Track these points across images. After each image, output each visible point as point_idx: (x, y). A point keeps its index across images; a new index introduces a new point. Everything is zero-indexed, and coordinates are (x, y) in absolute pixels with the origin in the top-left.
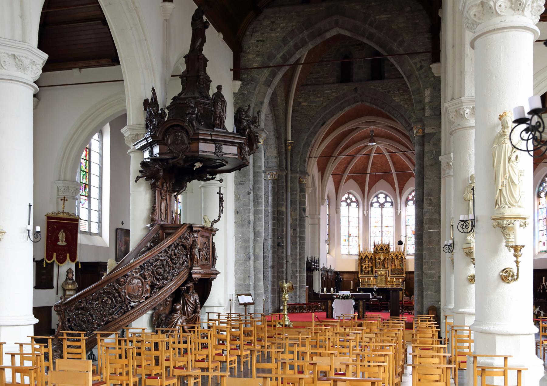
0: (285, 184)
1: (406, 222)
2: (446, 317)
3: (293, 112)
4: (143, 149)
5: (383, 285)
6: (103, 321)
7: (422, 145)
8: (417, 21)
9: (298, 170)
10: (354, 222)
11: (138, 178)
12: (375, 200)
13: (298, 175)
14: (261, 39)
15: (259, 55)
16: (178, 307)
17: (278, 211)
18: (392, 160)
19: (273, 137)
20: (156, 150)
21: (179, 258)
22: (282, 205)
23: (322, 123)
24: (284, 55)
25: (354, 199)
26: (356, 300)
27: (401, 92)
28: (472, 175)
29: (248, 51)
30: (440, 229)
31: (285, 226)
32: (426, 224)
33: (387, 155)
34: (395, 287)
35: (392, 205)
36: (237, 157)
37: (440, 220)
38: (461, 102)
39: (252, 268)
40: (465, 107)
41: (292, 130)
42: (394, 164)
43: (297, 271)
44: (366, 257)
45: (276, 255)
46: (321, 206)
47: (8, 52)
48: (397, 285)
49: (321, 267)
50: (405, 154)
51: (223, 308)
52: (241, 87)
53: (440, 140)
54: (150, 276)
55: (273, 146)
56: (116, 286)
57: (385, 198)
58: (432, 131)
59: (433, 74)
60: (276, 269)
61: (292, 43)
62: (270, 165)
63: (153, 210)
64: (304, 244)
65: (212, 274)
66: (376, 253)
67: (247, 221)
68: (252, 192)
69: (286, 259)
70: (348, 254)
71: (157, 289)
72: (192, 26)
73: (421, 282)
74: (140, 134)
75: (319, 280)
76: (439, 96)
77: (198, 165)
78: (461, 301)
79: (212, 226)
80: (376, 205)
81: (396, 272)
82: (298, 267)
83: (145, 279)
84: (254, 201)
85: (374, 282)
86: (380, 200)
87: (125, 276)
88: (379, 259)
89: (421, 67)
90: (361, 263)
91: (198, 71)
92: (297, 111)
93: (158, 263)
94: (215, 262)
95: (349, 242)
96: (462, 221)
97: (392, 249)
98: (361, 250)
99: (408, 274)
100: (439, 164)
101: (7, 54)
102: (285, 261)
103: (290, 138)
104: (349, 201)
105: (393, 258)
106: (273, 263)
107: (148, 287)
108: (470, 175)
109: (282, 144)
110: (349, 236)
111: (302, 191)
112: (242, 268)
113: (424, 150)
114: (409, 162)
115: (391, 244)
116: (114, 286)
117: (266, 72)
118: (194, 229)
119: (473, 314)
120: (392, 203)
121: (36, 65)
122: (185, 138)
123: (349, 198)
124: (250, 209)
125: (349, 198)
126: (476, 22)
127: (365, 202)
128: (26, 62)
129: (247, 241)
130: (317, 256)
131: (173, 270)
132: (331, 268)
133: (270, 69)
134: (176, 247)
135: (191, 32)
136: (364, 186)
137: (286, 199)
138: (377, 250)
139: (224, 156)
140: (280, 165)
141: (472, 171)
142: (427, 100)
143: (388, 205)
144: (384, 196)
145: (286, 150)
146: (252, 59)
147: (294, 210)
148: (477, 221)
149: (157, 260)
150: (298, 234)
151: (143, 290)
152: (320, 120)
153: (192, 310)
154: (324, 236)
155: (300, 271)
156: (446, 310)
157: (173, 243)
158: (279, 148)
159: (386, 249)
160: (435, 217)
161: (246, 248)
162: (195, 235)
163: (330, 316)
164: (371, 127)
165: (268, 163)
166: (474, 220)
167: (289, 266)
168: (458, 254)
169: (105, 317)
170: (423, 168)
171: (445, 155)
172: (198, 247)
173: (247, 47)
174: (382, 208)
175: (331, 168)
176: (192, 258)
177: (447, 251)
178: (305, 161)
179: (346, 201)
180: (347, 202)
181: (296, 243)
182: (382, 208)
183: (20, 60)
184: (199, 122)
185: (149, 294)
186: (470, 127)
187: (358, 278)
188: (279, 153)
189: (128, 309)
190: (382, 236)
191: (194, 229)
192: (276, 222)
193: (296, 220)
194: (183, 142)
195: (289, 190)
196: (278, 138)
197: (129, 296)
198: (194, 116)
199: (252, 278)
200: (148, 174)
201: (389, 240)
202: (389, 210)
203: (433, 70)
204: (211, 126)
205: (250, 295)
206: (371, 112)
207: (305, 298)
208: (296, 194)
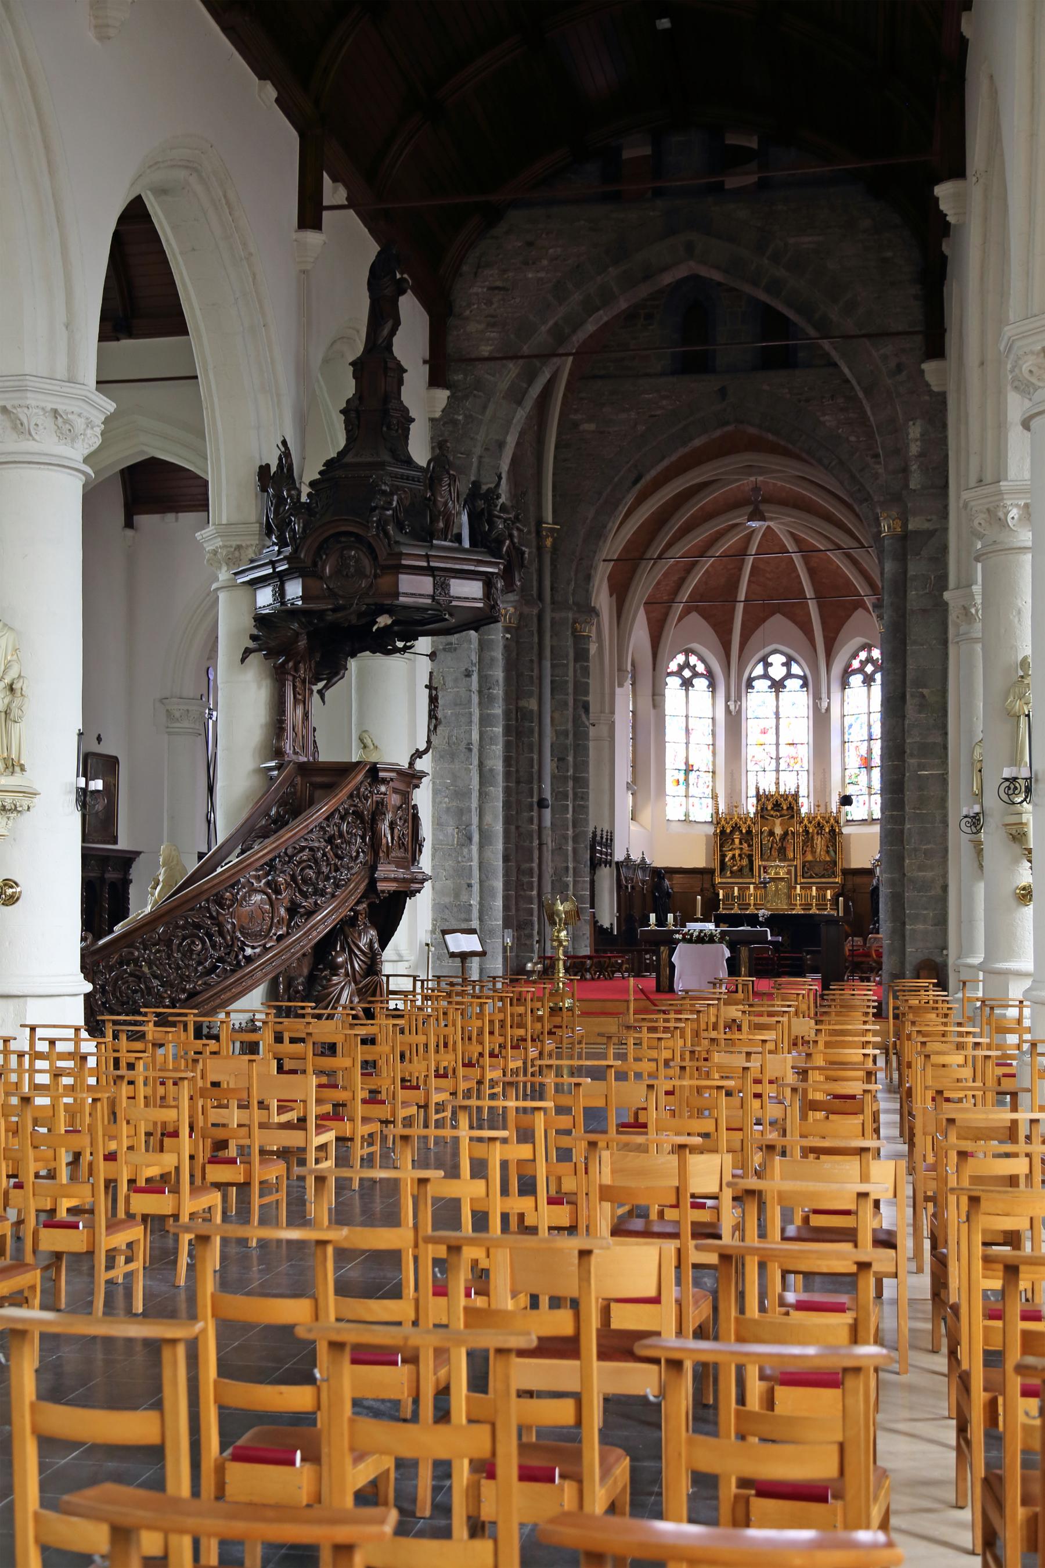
0: (536, 639)
1: (843, 733)
2: (964, 983)
3: (557, 447)
4: (256, 583)
5: (781, 906)
6: (184, 991)
7: (902, 558)
8: (889, 254)
9: (571, 602)
11: (247, 652)
12: (759, 670)
13: (570, 615)
14: (499, 284)
15: (494, 325)
16: (340, 960)
17: (518, 709)
20: (294, 589)
21: (349, 843)
22: (530, 694)
24: (556, 324)
25: (701, 668)
26: (732, 947)
28: (1025, 658)
29: (468, 312)
30: (946, 769)
31: (536, 749)
32: (912, 755)
33: (797, 558)
34: (814, 911)
35: (805, 685)
36: (481, 605)
37: (945, 748)
38: (1000, 493)
39: (475, 864)
40: (1009, 503)
41: (554, 496)
42: (812, 572)
43: (567, 868)
44: (736, 828)
45: (513, 828)
46: (618, 690)
47: (43, 404)
48: (821, 906)
49: (619, 856)
50: (848, 556)
51: (406, 964)
52: (449, 404)
53: (944, 549)
54: (288, 885)
56: (214, 908)
57: (787, 665)
58: (926, 526)
59: (928, 385)
60: (512, 864)
61: (577, 297)
63: (278, 726)
64: (585, 797)
65: (414, 880)
67: (463, 746)
68: (475, 669)
69: (540, 838)
70: (687, 821)
71: (302, 916)
72: (369, 289)
73: (898, 900)
74: (247, 546)
75: (611, 892)
76: (944, 441)
77: (384, 620)
78: (999, 942)
79: (411, 764)
80: (761, 685)
81: (817, 870)
82: (570, 858)
83: (278, 892)
84: (480, 692)
85: (755, 899)
87: (232, 886)
88: (771, 833)
89: (899, 368)
90: (722, 846)
91: (386, 400)
93: (305, 855)
94: (420, 852)
95: (687, 785)
96: (1007, 780)
97: (806, 807)
98: (722, 808)
99: (850, 877)
100: (943, 608)
101: (43, 409)
102: (536, 843)
103: (549, 516)
104: (687, 673)
105: (807, 832)
107: (282, 911)
108: (1020, 658)
110: (689, 769)
111: (582, 655)
112: (450, 863)
113: (905, 572)
114: (853, 569)
115: (803, 792)
116: (208, 910)
117: (513, 369)
118: (381, 774)
119: (1027, 975)
120: (804, 678)
121: (92, 428)
122: (366, 563)
123: (687, 665)
124: (470, 713)
125: (687, 665)
126: (1033, 384)
127: (733, 685)
128: (79, 424)
129: (461, 794)
130: (606, 827)
131: (336, 871)
133: (521, 362)
134: (343, 818)
135: (367, 302)
136: (730, 631)
137: (540, 678)
139: (454, 603)
141: (1025, 648)
142: (914, 449)
143: (793, 684)
144: (784, 659)
145: (540, 548)
146: (477, 333)
147: (559, 706)
148: (1037, 780)
149: (303, 849)
150: (571, 773)
151: (272, 919)
153: (364, 966)
154: (623, 773)
155: (574, 869)
156: (962, 969)
157: (337, 810)
159: (790, 808)
160: (935, 738)
161: (461, 813)
162: (383, 789)
163: (666, 986)
164: (753, 479)
166: (1030, 778)
167: (548, 856)
168: (992, 837)
169: (188, 982)
170: (903, 616)
171: (957, 588)
172: (389, 816)
173: (464, 304)
174: (777, 692)
175: (643, 587)
176: (375, 845)
177: (968, 830)
179: (679, 673)
180: (682, 677)
182: (777, 692)
183: (66, 422)
184: (400, 527)
185: (285, 929)
186: (1020, 548)
187: (713, 885)
189: (239, 962)
190: (777, 771)
191: (381, 774)
193: (566, 734)
194: (361, 573)
195: (548, 653)
197: (241, 933)
198: (390, 512)
199: (476, 888)
200: (272, 644)
201: (796, 780)
202: (796, 700)
203: (930, 378)
204: (426, 535)
205: (472, 931)
206: (755, 445)
207: (588, 942)
208: (567, 665)
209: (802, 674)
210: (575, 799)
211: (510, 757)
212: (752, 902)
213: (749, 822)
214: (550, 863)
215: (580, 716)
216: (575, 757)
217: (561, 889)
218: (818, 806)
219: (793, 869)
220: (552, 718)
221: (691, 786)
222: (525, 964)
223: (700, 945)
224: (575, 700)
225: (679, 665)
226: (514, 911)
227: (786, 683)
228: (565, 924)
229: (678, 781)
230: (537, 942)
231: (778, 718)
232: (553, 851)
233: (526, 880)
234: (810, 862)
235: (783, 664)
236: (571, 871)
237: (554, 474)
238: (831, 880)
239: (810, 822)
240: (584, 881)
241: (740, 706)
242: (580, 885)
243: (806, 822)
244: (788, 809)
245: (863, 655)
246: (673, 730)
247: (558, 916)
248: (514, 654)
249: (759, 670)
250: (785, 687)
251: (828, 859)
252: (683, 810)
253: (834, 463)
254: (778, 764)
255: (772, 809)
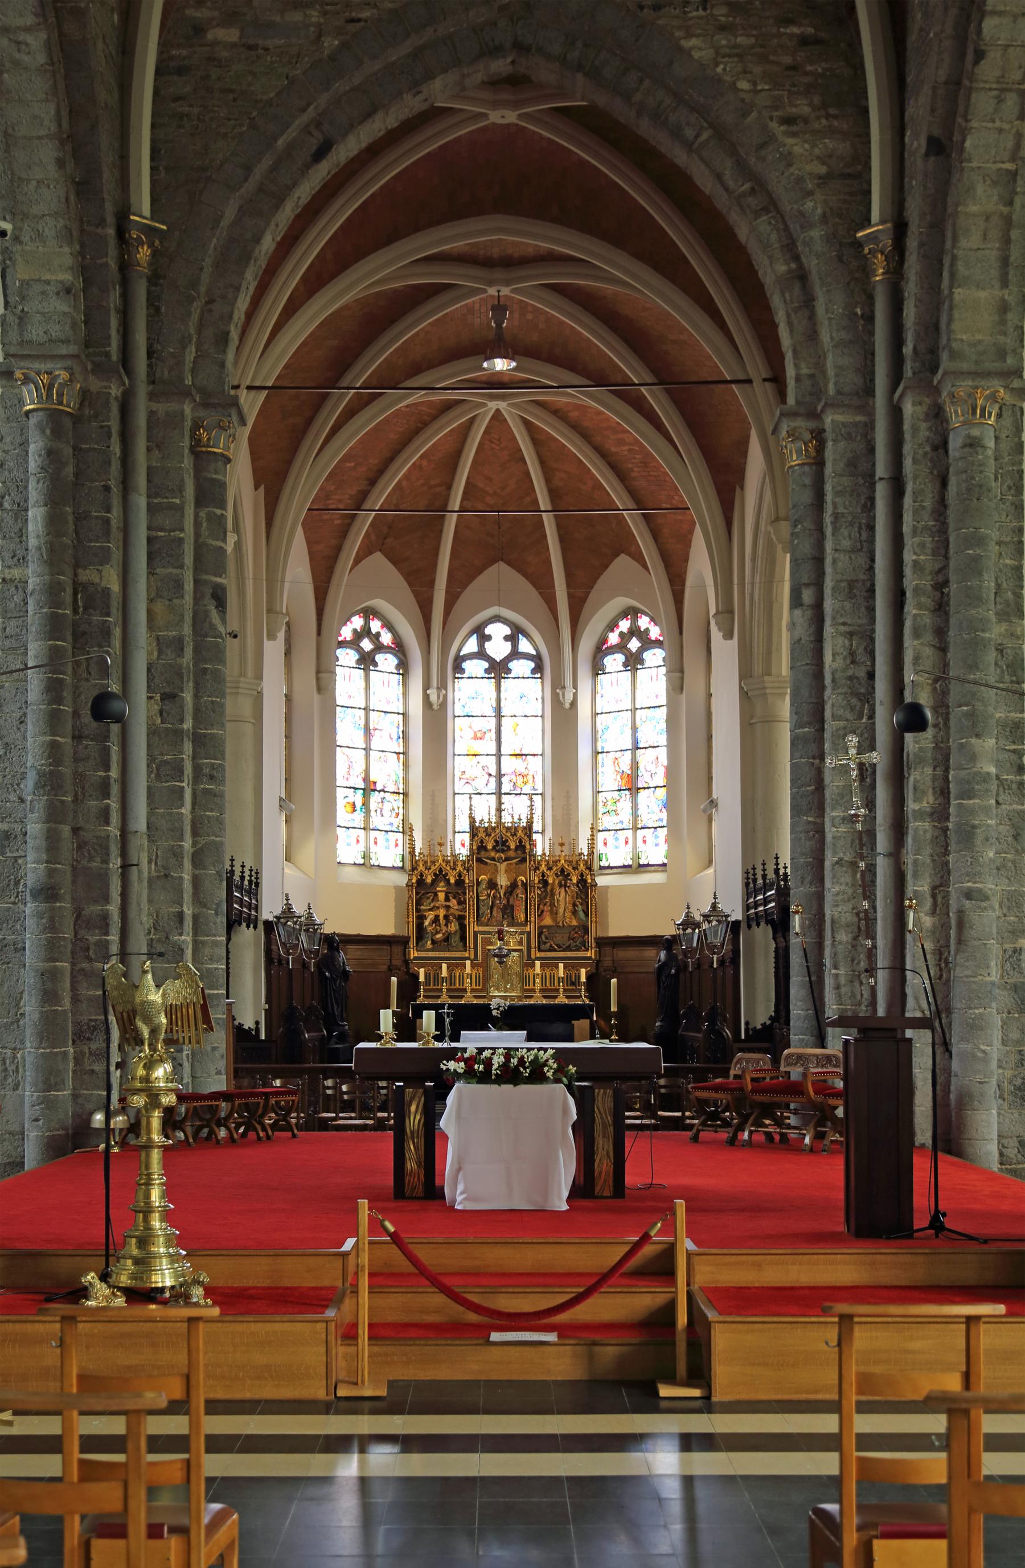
0: (116, 448)
3: (158, 72)
9: (189, 381)
10: (387, 732)
12: (471, 645)
18: (548, 481)
19: (52, 171)
22: (104, 558)
23: (313, 143)
25: (386, 638)
27: (720, 12)
34: (562, 1000)
35: (539, 668)
43: (180, 916)
44: (440, 876)
45: (66, 830)
49: (269, 909)
55: (50, 228)
57: (512, 638)
62: (35, 332)
66: (479, 860)
69: (124, 853)
70: (366, 864)
80: (475, 667)
86: (490, 648)
88: (492, 885)
90: (419, 903)
92: (181, 71)
97: (541, 846)
99: (608, 950)
102: (115, 863)
104: (367, 645)
105: (545, 883)
106: (51, 873)
109: (102, 222)
110: (369, 788)
123: (366, 632)
125: (366, 632)
132: (310, 916)
136: (432, 583)
137: (126, 530)
138: (482, 847)
140: (91, 341)
143: (521, 667)
144: (507, 631)
145: (125, 267)
147: (166, 590)
150: (188, 725)
152: (306, 130)
155: (195, 918)
158: (83, 238)
159: (521, 847)
165: (23, 319)
167: (140, 890)
178: (223, 340)
180: (359, 650)
181: (178, 771)
188: (87, 272)
192: (66, 644)
193: (178, 645)
195: (141, 480)
196: (84, 188)
202: (525, 692)
207: (222, 1065)
208: (180, 509)
209: (534, 653)
210: (197, 778)
211: (61, 681)
212: (538, 986)
213: (459, 868)
214: (145, 905)
215: (207, 614)
216: (196, 696)
217: (165, 956)
218: (562, 845)
219: (525, 937)
220: (150, 613)
221: (373, 813)
222: (91, 1114)
223: (508, 1088)
224: (196, 582)
225: (355, 630)
226: (67, 1003)
227: (511, 665)
228: (169, 1042)
229: (354, 805)
230: (118, 1066)
231: (499, 716)
232: (151, 881)
233: (93, 938)
234: (548, 927)
235: (506, 638)
236: (188, 922)
237: (153, 126)
238: (580, 954)
239: (550, 869)
240: (216, 944)
241: (445, 696)
242: (207, 951)
243: (543, 868)
244: (517, 847)
245: (624, 625)
246: (347, 729)
247: (148, 1019)
248: (69, 470)
249: (471, 645)
250: (509, 671)
251: (574, 923)
252: (361, 847)
253: (704, 136)
254: (499, 784)
255: (494, 848)
